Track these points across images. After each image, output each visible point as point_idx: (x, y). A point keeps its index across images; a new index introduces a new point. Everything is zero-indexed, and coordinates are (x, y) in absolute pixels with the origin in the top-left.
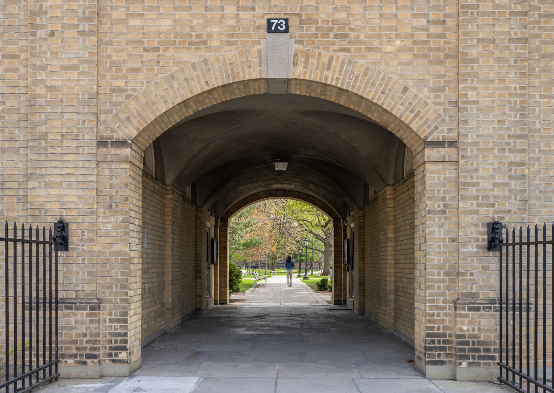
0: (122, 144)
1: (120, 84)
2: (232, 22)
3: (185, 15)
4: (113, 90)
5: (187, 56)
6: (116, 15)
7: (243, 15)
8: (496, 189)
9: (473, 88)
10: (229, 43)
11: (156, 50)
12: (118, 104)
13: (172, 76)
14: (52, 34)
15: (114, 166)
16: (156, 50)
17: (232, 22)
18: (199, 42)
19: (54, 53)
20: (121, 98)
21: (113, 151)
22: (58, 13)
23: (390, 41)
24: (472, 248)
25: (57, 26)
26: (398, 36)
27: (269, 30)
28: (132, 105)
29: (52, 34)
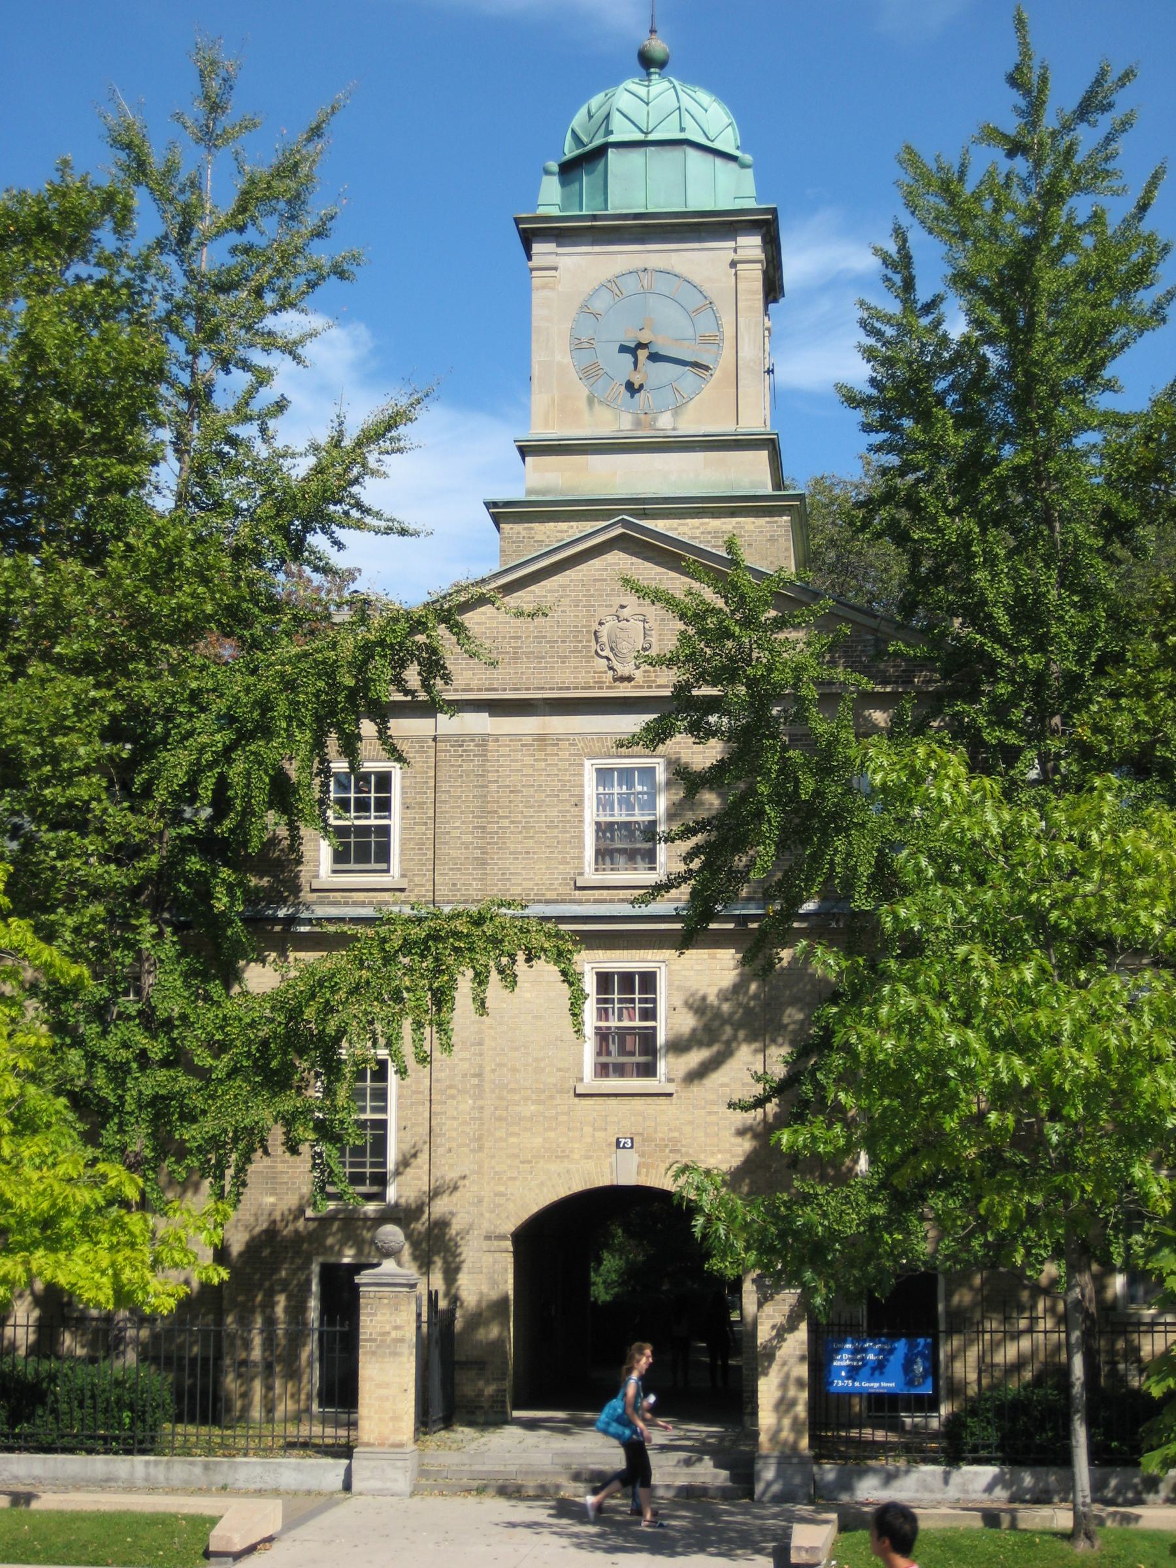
0: (501, 1237)
1: (502, 1189)
2: (589, 1140)
3: (552, 1134)
4: (496, 1195)
5: (554, 1167)
6: (498, 1134)
7: (598, 1134)
8: (131, 540)
9: (806, 1199)
10: (588, 1157)
11: (529, 1162)
12: (499, 1205)
13: (542, 1183)
14: (450, 1151)
15: (497, 1255)
16: (529, 1162)
17: (589, 1140)
18: (564, 1156)
19: (451, 1166)
20: (502, 1200)
21: (496, 1243)
22: (454, 1134)
23: (713, 1154)
24: (631, 1019)
25: (454, 1145)
26: (719, 1151)
27: (618, 1146)
28: (511, 1206)
29: (450, 1151)
